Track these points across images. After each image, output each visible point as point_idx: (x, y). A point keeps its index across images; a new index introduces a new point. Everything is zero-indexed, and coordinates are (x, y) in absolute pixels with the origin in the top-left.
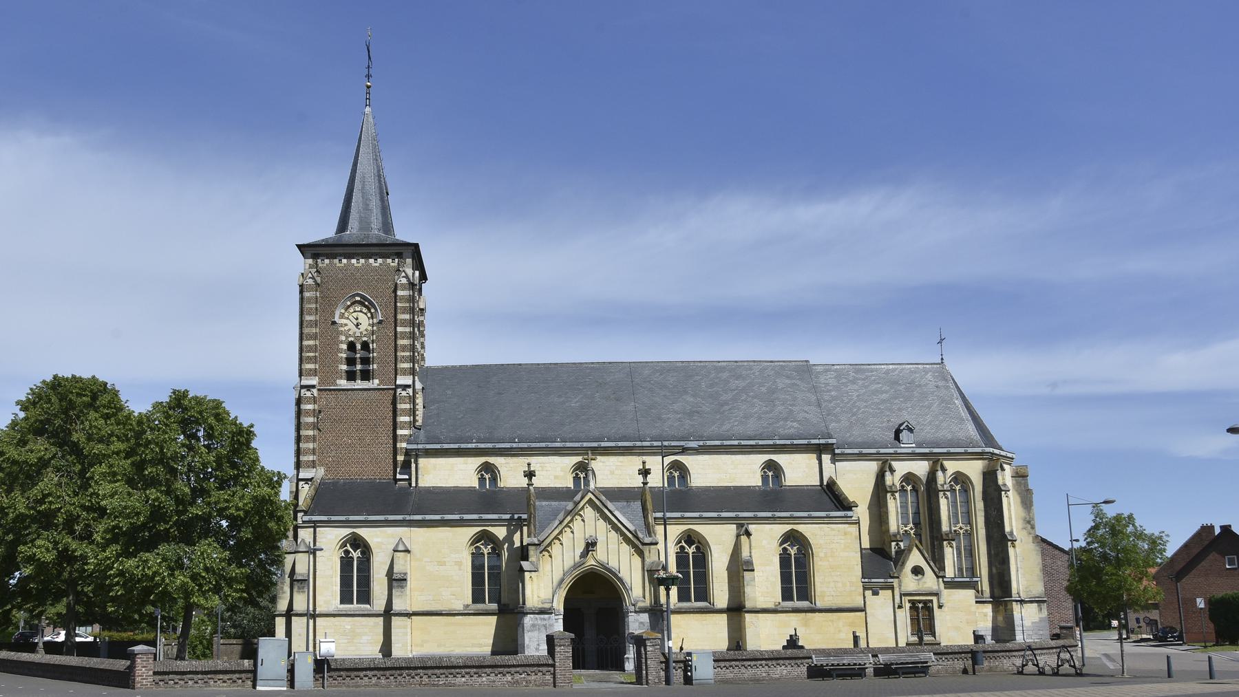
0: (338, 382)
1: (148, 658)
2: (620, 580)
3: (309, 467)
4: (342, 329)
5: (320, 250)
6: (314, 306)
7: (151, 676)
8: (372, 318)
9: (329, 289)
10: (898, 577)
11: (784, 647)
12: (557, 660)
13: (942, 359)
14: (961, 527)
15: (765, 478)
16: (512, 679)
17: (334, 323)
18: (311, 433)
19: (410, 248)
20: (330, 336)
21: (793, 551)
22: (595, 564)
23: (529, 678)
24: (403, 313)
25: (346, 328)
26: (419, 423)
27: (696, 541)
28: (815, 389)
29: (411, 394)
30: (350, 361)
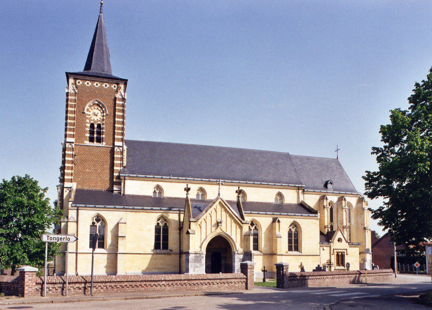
0: (85, 142)
1: (33, 274)
2: (232, 239)
3: (69, 182)
4: (87, 116)
5: (77, 77)
6: (74, 103)
7: (35, 286)
8: (103, 113)
9: (82, 96)
10: (333, 242)
11: (314, 270)
12: (248, 276)
13: (337, 158)
14: (348, 224)
15: (276, 199)
16: (228, 285)
17: (84, 113)
18: (70, 165)
19: (123, 81)
20: (82, 119)
21: (293, 230)
22: (221, 232)
23: (236, 285)
24: (119, 112)
25: (90, 116)
26: (125, 164)
27: (255, 224)
28: (293, 165)
29: (122, 151)
30: (92, 132)
